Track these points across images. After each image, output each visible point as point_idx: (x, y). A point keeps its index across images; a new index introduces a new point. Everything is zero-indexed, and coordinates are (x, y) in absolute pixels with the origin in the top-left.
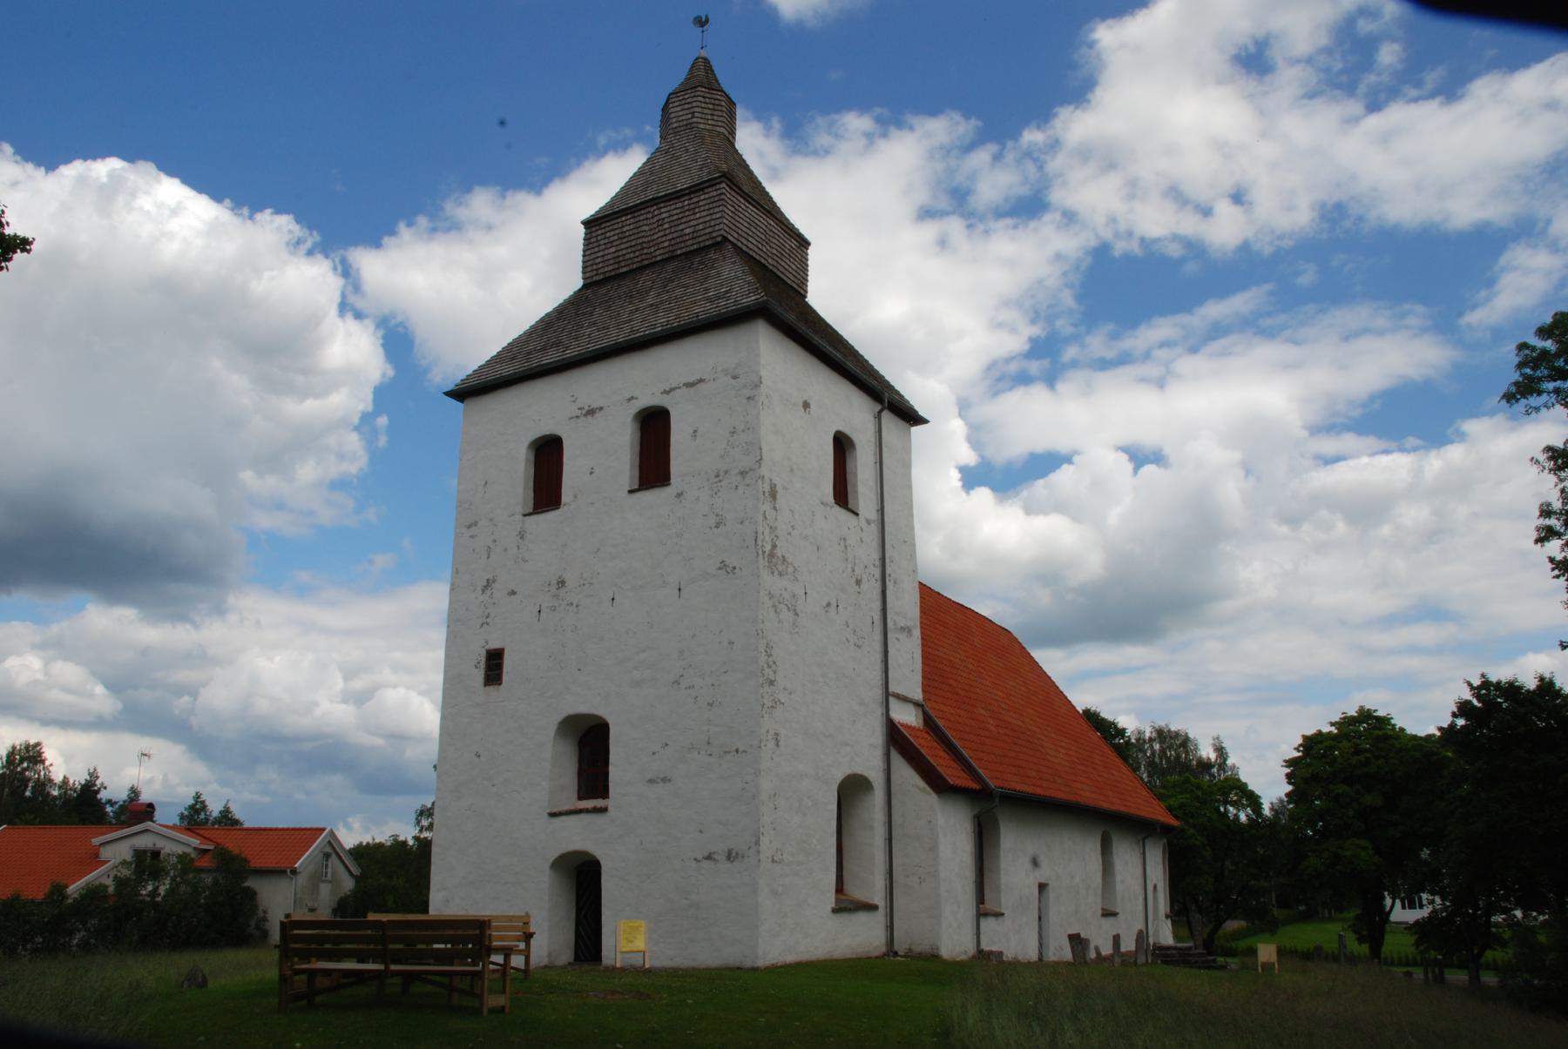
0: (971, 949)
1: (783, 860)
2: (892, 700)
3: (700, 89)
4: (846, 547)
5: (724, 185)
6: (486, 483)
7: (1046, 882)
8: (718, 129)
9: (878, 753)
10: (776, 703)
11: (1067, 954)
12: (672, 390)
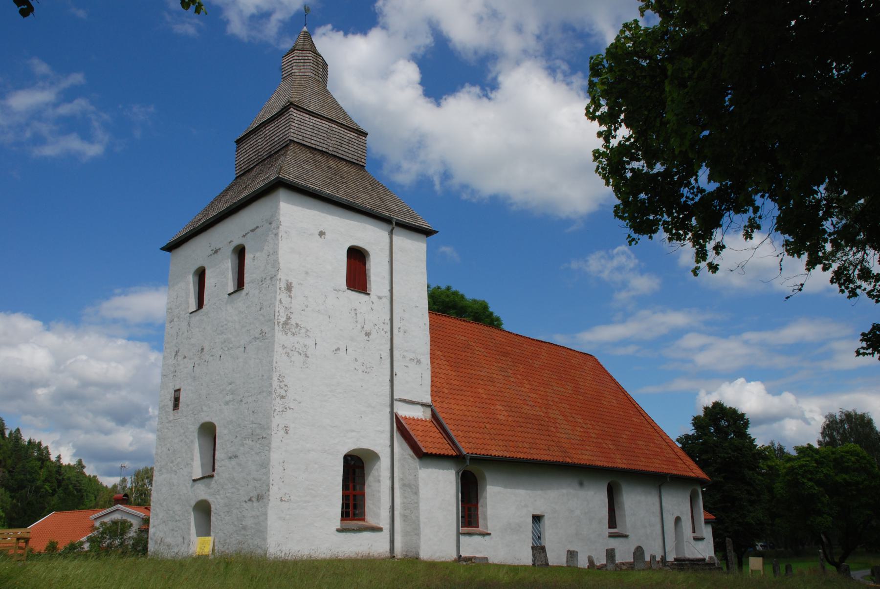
0: (454, 556)
1: (290, 500)
2: (396, 404)
3: (296, 51)
4: (356, 314)
5: (292, 109)
8: (307, 74)
9: (387, 435)
10: (286, 409)
12: (246, 234)
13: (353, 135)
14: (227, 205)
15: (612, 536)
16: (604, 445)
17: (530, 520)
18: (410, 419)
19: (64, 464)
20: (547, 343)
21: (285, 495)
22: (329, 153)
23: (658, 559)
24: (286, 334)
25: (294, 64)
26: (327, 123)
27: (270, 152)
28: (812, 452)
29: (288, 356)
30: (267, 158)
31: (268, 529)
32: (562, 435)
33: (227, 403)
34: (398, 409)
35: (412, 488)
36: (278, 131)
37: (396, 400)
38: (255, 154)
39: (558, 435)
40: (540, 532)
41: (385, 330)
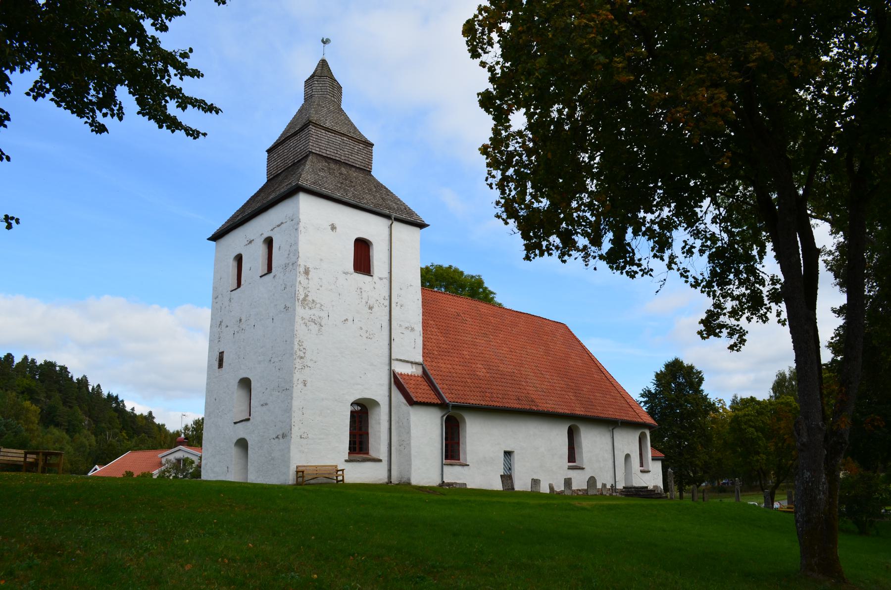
3: (315, 77)
4: (361, 292)
6: (221, 278)
7: (513, 450)
9: (386, 388)
10: (304, 367)
11: (548, 491)
12: (274, 228)
13: (361, 146)
14: (259, 205)
15: (570, 468)
16: (567, 396)
17: (502, 454)
18: (405, 375)
19: (137, 414)
20: (525, 313)
23: (608, 487)
24: (305, 308)
26: (340, 137)
27: (294, 161)
29: (306, 326)
30: (291, 165)
31: (291, 459)
32: (531, 388)
33: (260, 362)
34: (395, 367)
35: (406, 430)
36: (300, 144)
37: (394, 360)
38: (282, 161)
39: (528, 388)
40: (510, 464)
41: (385, 304)
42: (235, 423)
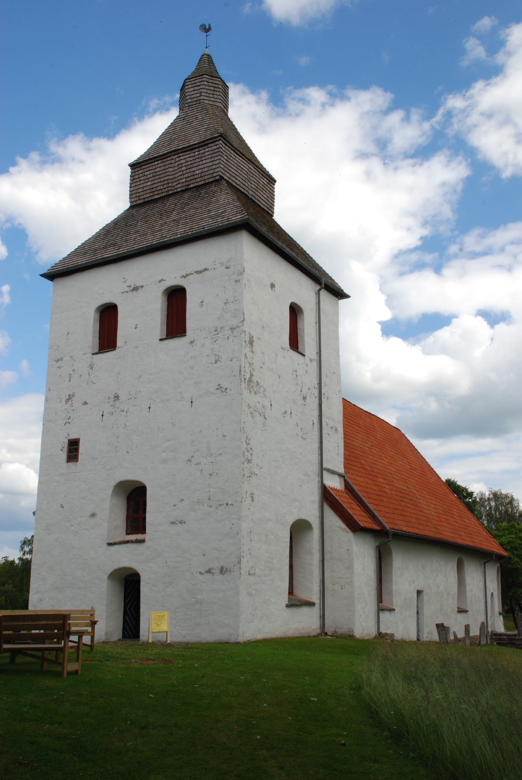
0: (373, 632)
10: (252, 474)
12: (188, 275)
21: (252, 568)
22: (248, 197)
25: (204, 90)
28: (516, 530)
42: (110, 544)
